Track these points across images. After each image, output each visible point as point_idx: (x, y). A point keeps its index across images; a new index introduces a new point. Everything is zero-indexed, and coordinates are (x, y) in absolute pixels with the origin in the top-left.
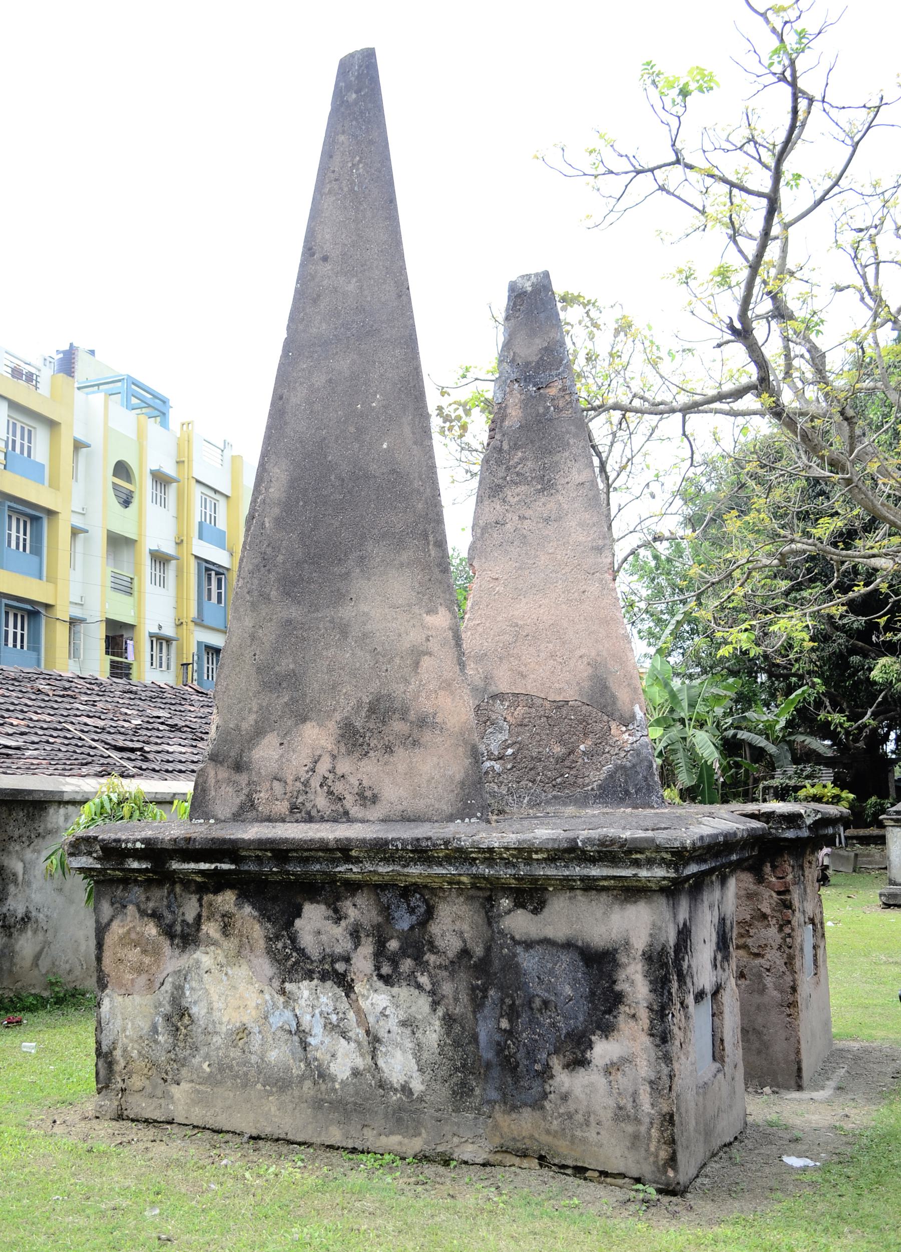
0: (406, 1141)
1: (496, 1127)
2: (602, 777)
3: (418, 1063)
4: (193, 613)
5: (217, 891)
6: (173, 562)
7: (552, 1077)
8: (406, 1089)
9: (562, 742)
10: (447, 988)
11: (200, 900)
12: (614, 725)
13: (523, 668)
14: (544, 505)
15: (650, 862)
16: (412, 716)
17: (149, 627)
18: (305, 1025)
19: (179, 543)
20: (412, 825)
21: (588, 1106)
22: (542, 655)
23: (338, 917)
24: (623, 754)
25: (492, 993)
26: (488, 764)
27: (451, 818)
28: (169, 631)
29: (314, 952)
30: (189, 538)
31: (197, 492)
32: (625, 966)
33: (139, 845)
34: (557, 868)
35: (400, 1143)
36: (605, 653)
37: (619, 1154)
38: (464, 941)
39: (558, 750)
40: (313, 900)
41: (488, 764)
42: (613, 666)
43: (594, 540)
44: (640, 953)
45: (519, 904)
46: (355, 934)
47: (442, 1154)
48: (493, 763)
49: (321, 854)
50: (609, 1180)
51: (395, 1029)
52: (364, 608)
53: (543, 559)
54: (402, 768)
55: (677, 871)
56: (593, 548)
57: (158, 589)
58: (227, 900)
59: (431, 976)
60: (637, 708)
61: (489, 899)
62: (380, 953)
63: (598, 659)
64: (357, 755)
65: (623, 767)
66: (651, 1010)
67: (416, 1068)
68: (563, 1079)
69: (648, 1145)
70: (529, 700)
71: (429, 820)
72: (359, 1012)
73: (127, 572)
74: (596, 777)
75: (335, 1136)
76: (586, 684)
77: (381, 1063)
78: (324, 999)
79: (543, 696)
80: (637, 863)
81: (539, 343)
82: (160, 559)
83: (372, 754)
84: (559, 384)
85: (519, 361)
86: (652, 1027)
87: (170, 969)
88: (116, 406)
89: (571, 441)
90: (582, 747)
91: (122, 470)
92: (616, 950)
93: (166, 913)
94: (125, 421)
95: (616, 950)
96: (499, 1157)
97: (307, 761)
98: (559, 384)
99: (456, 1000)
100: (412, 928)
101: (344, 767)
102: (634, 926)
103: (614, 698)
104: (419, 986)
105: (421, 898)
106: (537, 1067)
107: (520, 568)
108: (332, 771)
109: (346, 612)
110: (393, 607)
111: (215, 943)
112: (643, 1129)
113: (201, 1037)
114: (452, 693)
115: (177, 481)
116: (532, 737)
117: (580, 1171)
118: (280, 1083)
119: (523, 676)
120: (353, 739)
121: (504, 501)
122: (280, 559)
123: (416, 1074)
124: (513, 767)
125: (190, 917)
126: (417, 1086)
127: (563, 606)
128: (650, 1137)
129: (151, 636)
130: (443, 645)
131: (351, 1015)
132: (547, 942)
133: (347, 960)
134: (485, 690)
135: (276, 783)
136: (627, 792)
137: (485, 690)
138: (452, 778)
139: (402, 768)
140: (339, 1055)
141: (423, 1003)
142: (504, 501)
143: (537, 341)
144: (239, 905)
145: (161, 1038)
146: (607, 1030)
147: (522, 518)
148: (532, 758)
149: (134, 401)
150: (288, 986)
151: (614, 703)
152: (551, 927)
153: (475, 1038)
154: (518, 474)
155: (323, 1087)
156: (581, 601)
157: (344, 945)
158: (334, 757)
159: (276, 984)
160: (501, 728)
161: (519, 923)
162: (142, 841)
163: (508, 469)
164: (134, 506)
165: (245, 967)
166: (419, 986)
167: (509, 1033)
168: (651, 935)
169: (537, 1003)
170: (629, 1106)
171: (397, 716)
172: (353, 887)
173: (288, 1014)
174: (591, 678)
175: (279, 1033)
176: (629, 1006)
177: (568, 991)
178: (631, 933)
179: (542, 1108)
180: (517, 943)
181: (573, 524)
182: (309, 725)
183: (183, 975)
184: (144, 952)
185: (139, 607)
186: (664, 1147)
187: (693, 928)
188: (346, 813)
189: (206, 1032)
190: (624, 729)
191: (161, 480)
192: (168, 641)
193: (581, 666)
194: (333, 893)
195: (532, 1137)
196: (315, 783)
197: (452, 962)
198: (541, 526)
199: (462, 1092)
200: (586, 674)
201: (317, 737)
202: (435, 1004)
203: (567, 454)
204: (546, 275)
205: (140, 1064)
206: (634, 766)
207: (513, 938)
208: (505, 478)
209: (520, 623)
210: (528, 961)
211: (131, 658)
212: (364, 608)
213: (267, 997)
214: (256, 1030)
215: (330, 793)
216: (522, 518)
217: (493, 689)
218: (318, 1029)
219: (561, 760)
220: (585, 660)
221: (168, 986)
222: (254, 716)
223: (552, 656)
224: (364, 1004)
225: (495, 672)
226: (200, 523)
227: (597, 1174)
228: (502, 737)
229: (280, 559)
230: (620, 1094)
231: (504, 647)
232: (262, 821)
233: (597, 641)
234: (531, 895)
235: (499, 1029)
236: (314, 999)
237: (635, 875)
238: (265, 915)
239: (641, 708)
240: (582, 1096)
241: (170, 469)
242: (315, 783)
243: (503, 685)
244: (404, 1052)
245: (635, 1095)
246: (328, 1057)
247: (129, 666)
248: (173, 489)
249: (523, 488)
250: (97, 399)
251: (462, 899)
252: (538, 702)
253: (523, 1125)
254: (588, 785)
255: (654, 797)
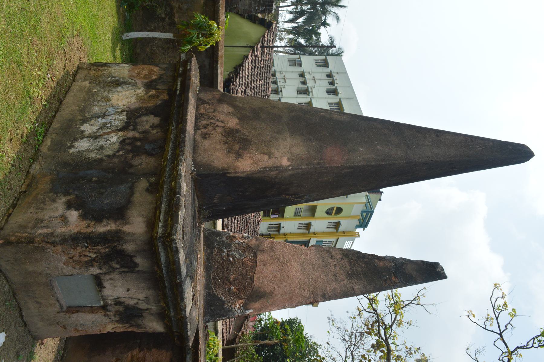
0: (47, 147)
1: (45, 176)
2: (219, 295)
3: (83, 151)
4: (290, 240)
5: (168, 94)
6: (307, 232)
7: (65, 196)
8: (72, 147)
9: (235, 280)
10: (116, 160)
11: (165, 89)
12: (243, 301)
13: (268, 265)
14: (342, 275)
15: (165, 226)
16: (241, 151)
17: (284, 223)
18: (106, 117)
19: (314, 233)
20: (192, 148)
21: (47, 209)
22: (274, 273)
23: (153, 127)
24: (229, 304)
25: (111, 175)
26: (225, 250)
27: (194, 160)
28: (282, 231)
29: (139, 120)
30: (317, 237)
31: (333, 239)
32: (115, 224)
33: (189, 67)
34: (167, 192)
35: (46, 145)
36: (276, 298)
37: (18, 221)
38: (137, 166)
39: (232, 278)
40: (161, 120)
41: (225, 250)
42: (270, 301)
43: (328, 294)
44: (121, 229)
45: (151, 184)
46: (145, 132)
47: (38, 158)
48: (226, 252)
49: (181, 116)
50: (6, 217)
51: (100, 144)
52: (289, 139)
53: (317, 274)
54: (218, 147)
55: (160, 237)
56: (324, 294)
57: (297, 226)
58: (165, 97)
59: (122, 155)
60: (251, 311)
61: (155, 174)
62: (135, 139)
63: (274, 295)
64: (224, 134)
65: (223, 304)
66: (90, 233)
67: (80, 150)
68: (62, 200)
69: (19, 232)
70: (254, 266)
71: (194, 154)
72: (110, 133)
73: (302, 214)
74: (219, 293)
75: (56, 125)
76: (262, 290)
77: (86, 139)
78: (117, 122)
79: (256, 272)
80: (166, 221)
81: (414, 274)
82: (308, 226)
83: (224, 138)
84: (397, 281)
85: (404, 266)
86: (81, 233)
87: (137, 81)
88: (361, 208)
89: (372, 286)
90: (233, 287)
91: (339, 210)
92: (124, 219)
93: (161, 81)
94: (357, 210)
95: (124, 219)
96: (30, 177)
97: (222, 119)
98: (397, 281)
99: (110, 163)
100: (145, 149)
101: (219, 130)
102: (136, 226)
103: (256, 301)
104: (118, 151)
105: (159, 149)
106: (71, 190)
107: (313, 264)
108: (217, 126)
109: (286, 134)
110: (290, 148)
111: (146, 93)
112: (29, 230)
113: (108, 89)
114: (252, 164)
115: (337, 232)
116: (237, 267)
117: (14, 206)
118: (83, 110)
119: (264, 265)
120: (230, 133)
121: (342, 259)
122: (308, 117)
123: (77, 150)
124: (224, 260)
125: (158, 87)
126: (72, 151)
127: (297, 282)
128: (23, 233)
129: (280, 224)
130: (274, 162)
131: (109, 130)
132: (132, 194)
133: (134, 130)
134: (258, 250)
135: (212, 110)
136: (211, 306)
137: (258, 250)
138: (213, 162)
139: (218, 147)
140: (92, 127)
141: (109, 152)
142: (342, 259)
143: (415, 273)
144: (162, 100)
145: (109, 79)
146: (83, 217)
147: (335, 266)
148: (228, 268)
149: (364, 215)
150: (126, 112)
151: (253, 301)
152: (139, 195)
153: (91, 169)
154: (354, 264)
155: (78, 122)
156: (299, 289)
157: (140, 128)
158: (223, 127)
159: (127, 109)
160: (241, 256)
161: (143, 184)
162: (190, 69)
163: (356, 260)
164: (326, 215)
165: (135, 101)
166: (118, 151)
167: (90, 181)
168: (129, 233)
169: (102, 190)
170: (43, 225)
171: (241, 146)
172: (166, 132)
173: (113, 112)
174: (265, 292)
175: (105, 110)
176: (94, 225)
177: (106, 202)
178: (131, 225)
179: (50, 192)
180: (133, 184)
181: (334, 286)
182: (238, 121)
183: (135, 85)
184: (146, 75)
185: (290, 219)
186: (16, 239)
187: (134, 275)
188: (199, 129)
189: (109, 91)
190: (241, 305)
191: (337, 225)
192: (279, 231)
193: (270, 288)
194: (164, 126)
195: (37, 188)
196: (212, 121)
197: (127, 162)
198: (332, 273)
199: (65, 165)
200: (266, 289)
201: (233, 123)
202: (109, 156)
203: (366, 284)
204: (445, 277)
205: (100, 73)
206: (224, 309)
207: (136, 182)
208: (352, 259)
209: (288, 264)
210: (123, 188)
211: (272, 217)
212: (289, 139)
213: (121, 107)
214: (108, 104)
215: (208, 125)
216: (335, 266)
217: (259, 253)
218: (104, 121)
219: (227, 279)
220: (273, 290)
221: (130, 81)
222: (241, 105)
223: (274, 276)
224: (113, 134)
225: (266, 254)
226: (322, 241)
227: (10, 212)
228: (237, 256)
229: (308, 116)
230: (49, 221)
231: (277, 258)
232: (197, 105)
233: (282, 295)
234: (154, 189)
235: (93, 177)
236: (119, 120)
237: (160, 221)
238: (156, 107)
239: (251, 313)
240: (52, 207)
241: (341, 229)
242: (212, 121)
243: (260, 257)
244: (89, 146)
245: (48, 227)
246: (91, 123)
247: (269, 216)
248: (333, 230)
249: (348, 266)
250: (364, 200)
251: (156, 165)
252: (253, 271)
253: (44, 185)
254: (215, 290)
255: (208, 317)
